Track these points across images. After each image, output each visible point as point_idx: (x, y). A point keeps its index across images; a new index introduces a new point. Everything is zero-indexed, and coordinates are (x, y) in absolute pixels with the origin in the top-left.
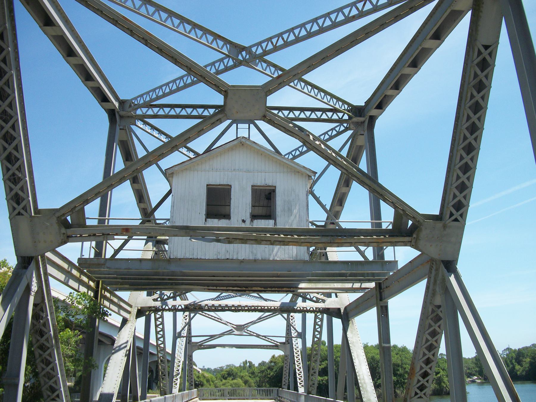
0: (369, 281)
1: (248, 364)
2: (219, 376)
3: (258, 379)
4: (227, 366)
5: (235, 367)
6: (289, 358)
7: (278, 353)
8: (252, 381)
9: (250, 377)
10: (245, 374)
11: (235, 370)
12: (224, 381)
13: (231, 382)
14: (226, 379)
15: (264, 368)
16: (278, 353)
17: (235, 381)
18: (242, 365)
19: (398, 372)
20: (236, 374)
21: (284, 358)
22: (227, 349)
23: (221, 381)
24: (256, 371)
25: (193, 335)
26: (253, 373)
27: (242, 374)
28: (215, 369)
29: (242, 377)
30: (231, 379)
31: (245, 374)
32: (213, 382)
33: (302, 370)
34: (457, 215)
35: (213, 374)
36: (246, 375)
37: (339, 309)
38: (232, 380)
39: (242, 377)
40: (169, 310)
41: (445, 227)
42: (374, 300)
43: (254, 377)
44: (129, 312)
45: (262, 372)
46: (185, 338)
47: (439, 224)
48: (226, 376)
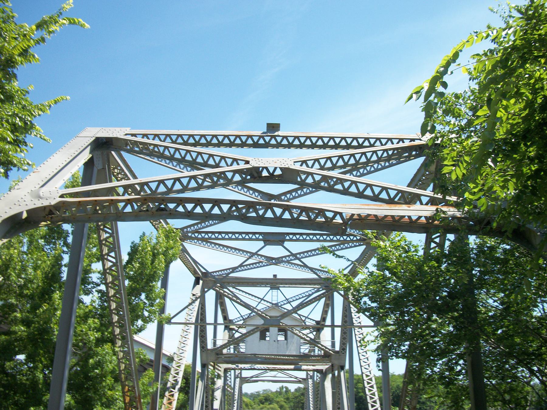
0: (508, 245)
1: (284, 389)
2: (257, 401)
3: (292, 404)
4: (264, 390)
5: (272, 392)
6: (306, 389)
7: (302, 386)
8: (287, 406)
9: (285, 402)
10: (281, 399)
11: (272, 396)
12: (262, 405)
13: (268, 407)
14: (263, 403)
15: (298, 394)
16: (302, 386)
17: (271, 406)
18: (279, 390)
19: (421, 400)
20: (273, 399)
21: (304, 389)
22: (266, 382)
23: (259, 405)
24: (291, 396)
25: (207, 322)
26: (288, 399)
27: (278, 400)
28: (252, 394)
29: (277, 402)
30: (267, 403)
31: (281, 399)
32: (251, 406)
33: (375, 390)
34: (343, 352)
35: (250, 399)
36: (281, 401)
37: (322, 370)
38: (269, 404)
39: (277, 402)
40: (239, 369)
41: (340, 355)
42: (331, 371)
43: (289, 403)
44: (220, 371)
45: (296, 397)
46: (193, 326)
47: (338, 355)
48: (264, 401)
